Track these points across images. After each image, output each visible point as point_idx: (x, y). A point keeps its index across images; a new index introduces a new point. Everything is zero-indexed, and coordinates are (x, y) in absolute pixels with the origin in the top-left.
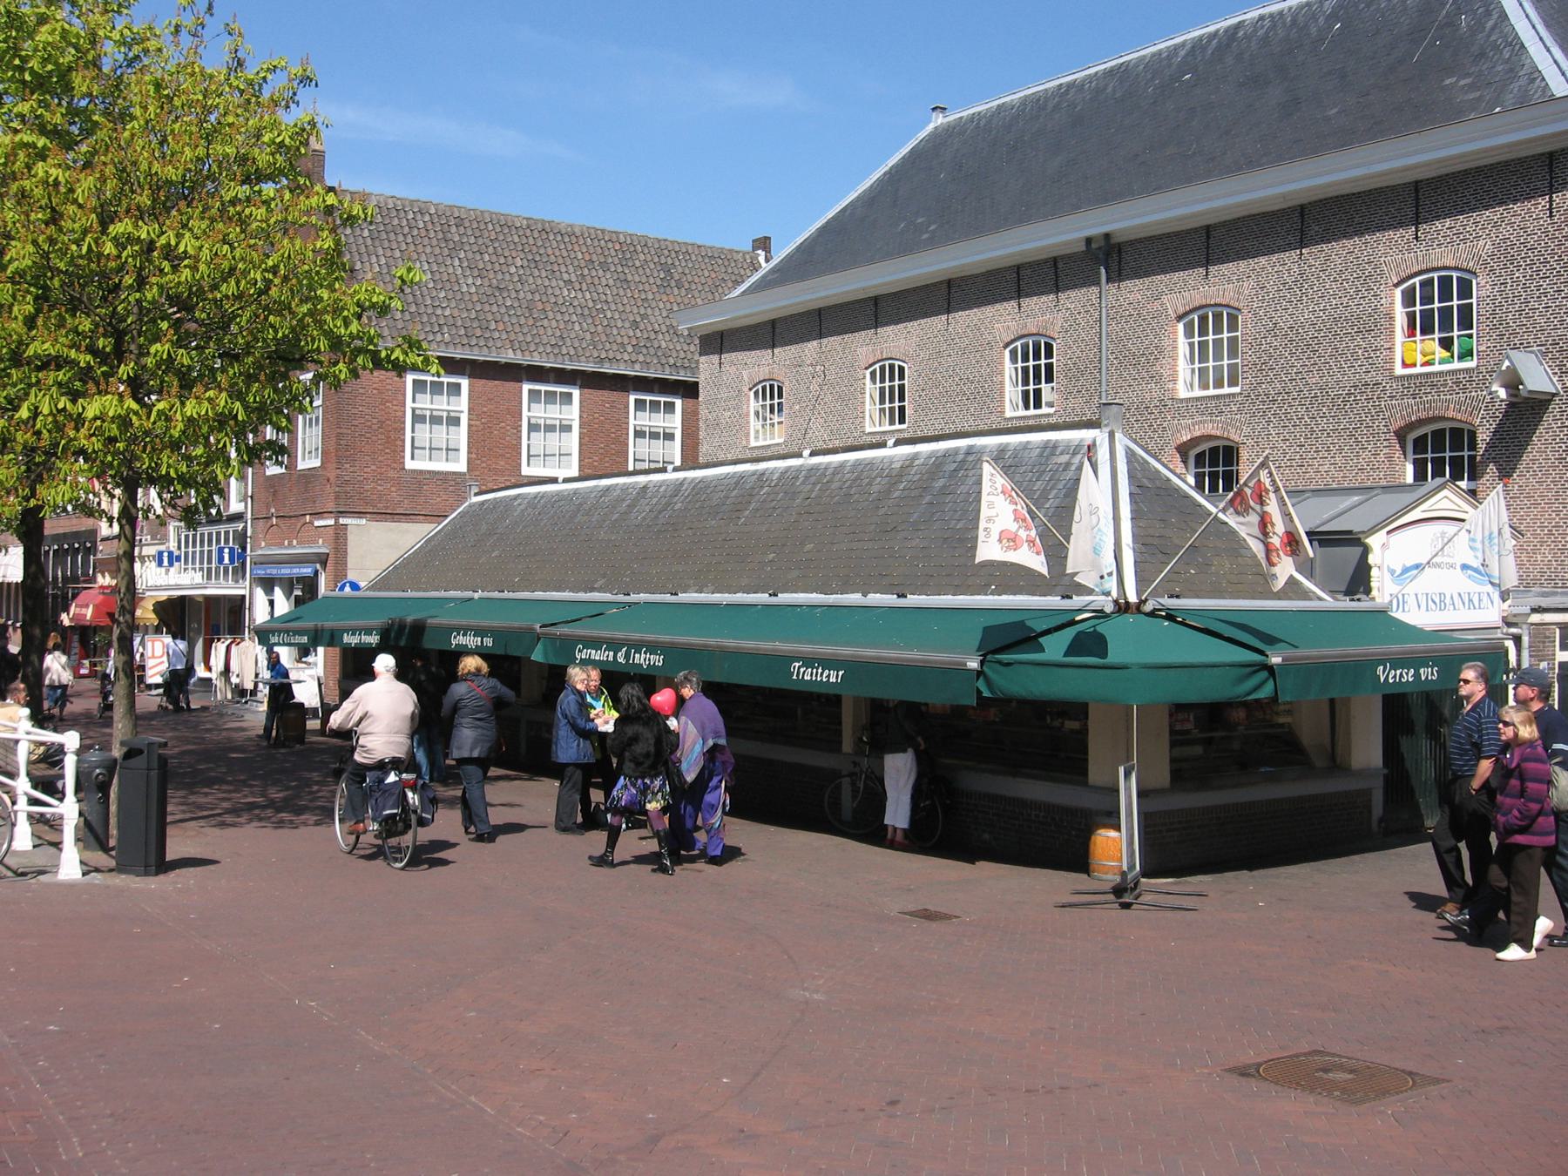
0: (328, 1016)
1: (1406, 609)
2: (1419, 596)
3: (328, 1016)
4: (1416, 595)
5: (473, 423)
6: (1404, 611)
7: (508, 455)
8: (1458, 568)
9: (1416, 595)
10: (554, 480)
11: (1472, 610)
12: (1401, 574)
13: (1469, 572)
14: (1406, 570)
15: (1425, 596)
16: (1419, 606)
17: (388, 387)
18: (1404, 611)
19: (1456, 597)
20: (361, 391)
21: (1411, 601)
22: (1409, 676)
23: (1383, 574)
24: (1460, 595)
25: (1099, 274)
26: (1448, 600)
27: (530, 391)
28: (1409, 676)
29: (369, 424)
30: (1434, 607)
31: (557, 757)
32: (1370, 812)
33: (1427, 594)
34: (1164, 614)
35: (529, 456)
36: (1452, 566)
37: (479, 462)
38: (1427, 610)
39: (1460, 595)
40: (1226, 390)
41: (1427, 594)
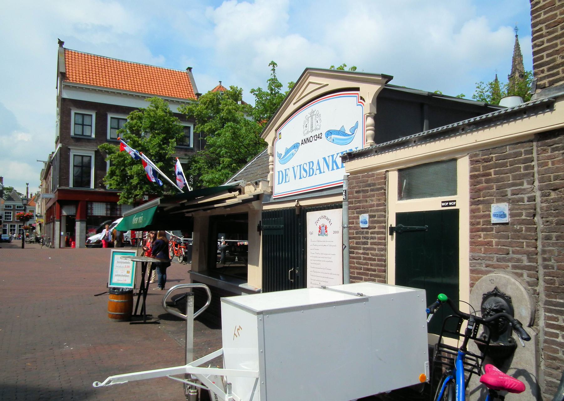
1: (287, 181)
2: (295, 168)
4: (293, 168)
11: (336, 171)
12: (285, 156)
14: (288, 151)
16: (295, 177)
19: (322, 162)
22: (457, 388)
23: (275, 159)
24: (324, 159)
25: (132, 243)
27: (111, 118)
28: (457, 388)
30: (305, 174)
34: (143, 314)
35: (119, 119)
36: (319, 137)
39: (324, 159)
40: (12, 214)
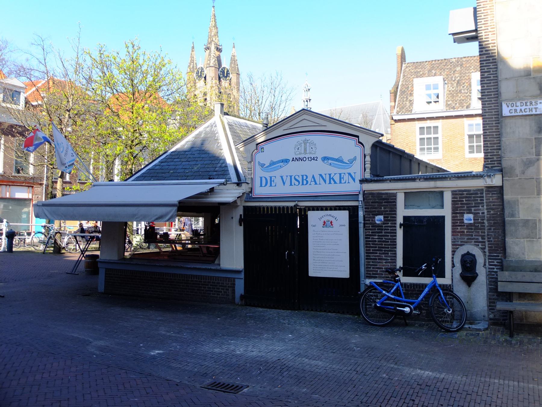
0: (184, 335)
3: (184, 335)
4: (282, 177)
5: (443, 140)
6: (271, 185)
7: (459, 150)
8: (319, 159)
9: (282, 177)
10: (142, 169)
13: (330, 161)
14: (272, 163)
15: (289, 177)
16: (284, 184)
17: (409, 131)
18: (271, 185)
20: (399, 134)
21: (278, 181)
26: (309, 179)
29: (402, 145)
31: (41, 250)
32: (234, 291)
33: (291, 176)
37: (447, 154)
38: (291, 185)
39: (321, 175)
41: (291, 176)
